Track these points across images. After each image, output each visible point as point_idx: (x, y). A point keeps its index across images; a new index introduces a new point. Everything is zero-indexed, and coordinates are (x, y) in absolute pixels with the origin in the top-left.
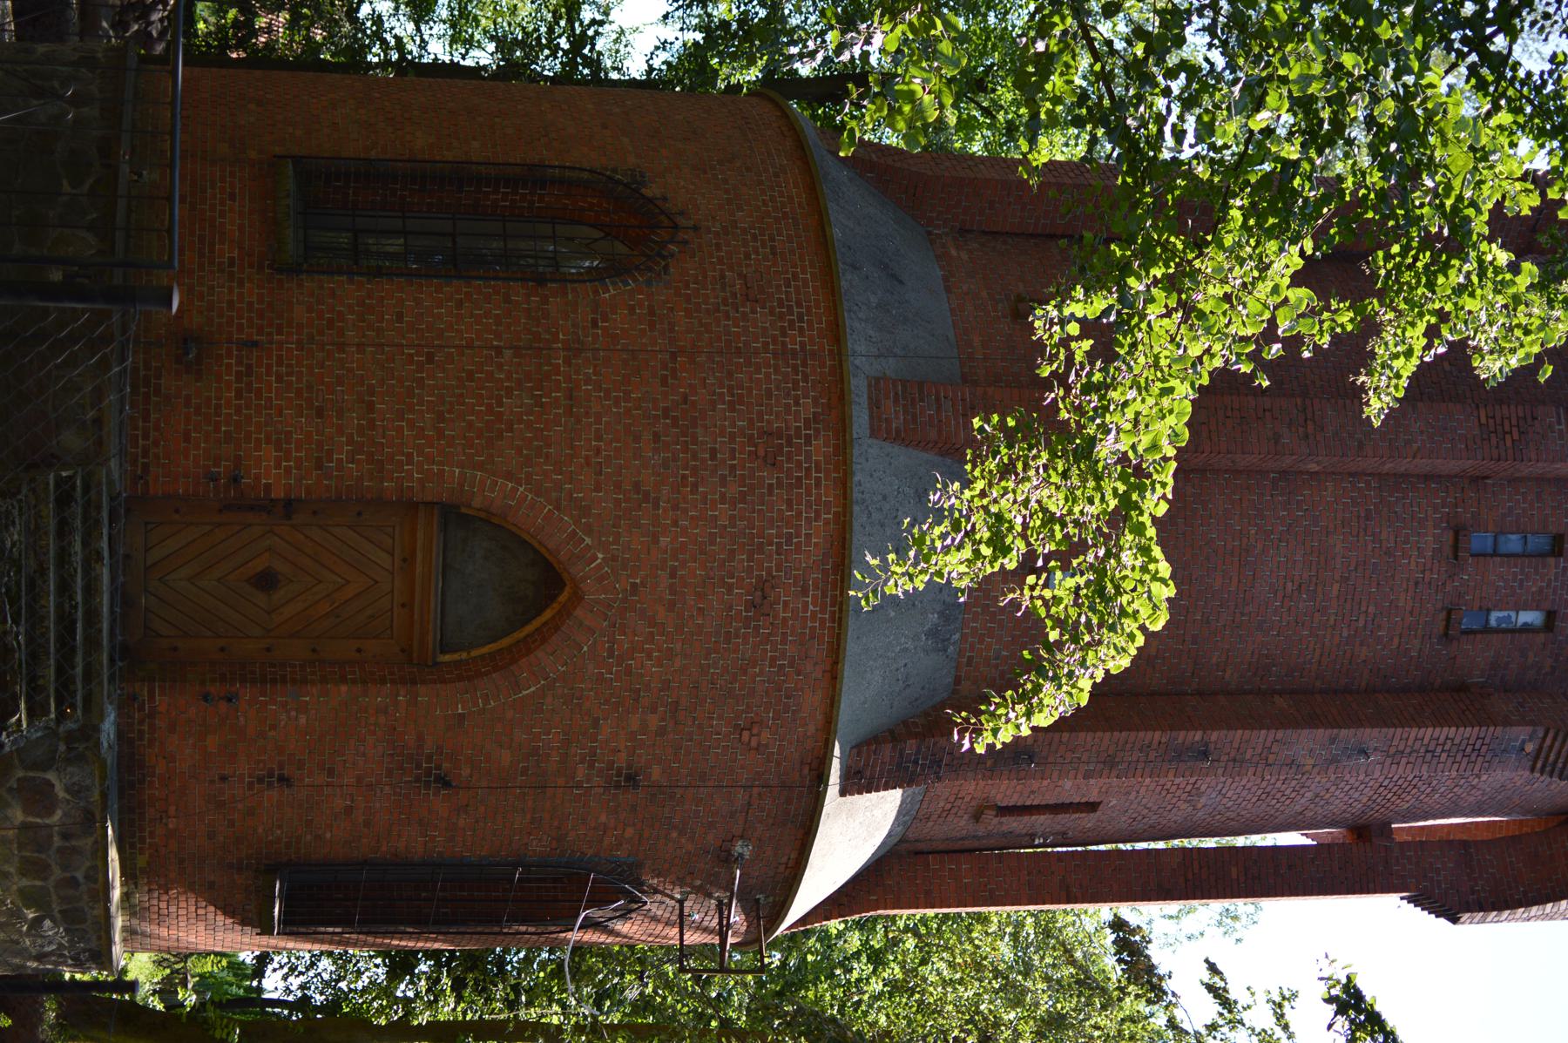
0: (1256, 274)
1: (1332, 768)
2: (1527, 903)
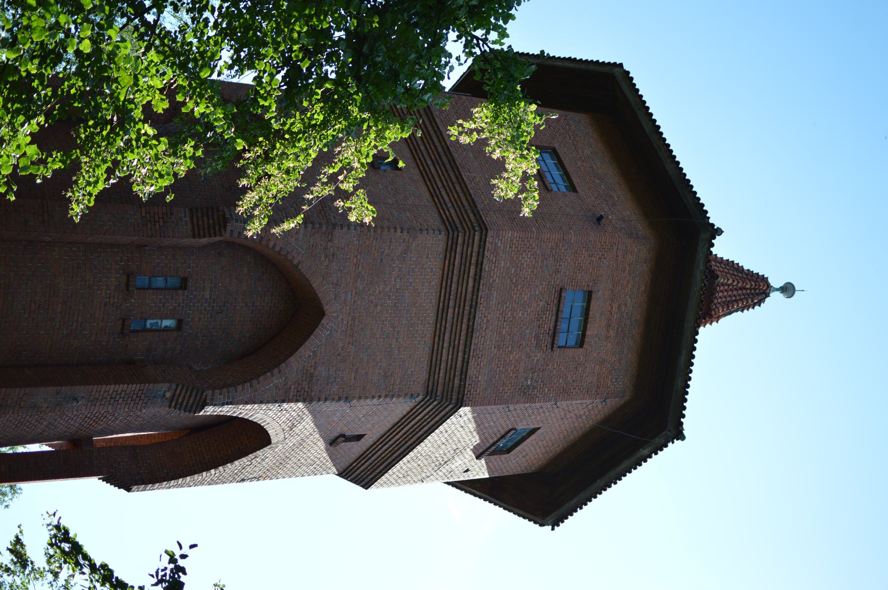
0: (11, 134)
1: (58, 408)
2: (169, 479)
